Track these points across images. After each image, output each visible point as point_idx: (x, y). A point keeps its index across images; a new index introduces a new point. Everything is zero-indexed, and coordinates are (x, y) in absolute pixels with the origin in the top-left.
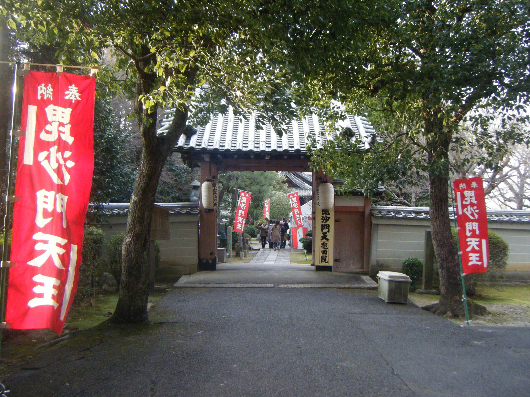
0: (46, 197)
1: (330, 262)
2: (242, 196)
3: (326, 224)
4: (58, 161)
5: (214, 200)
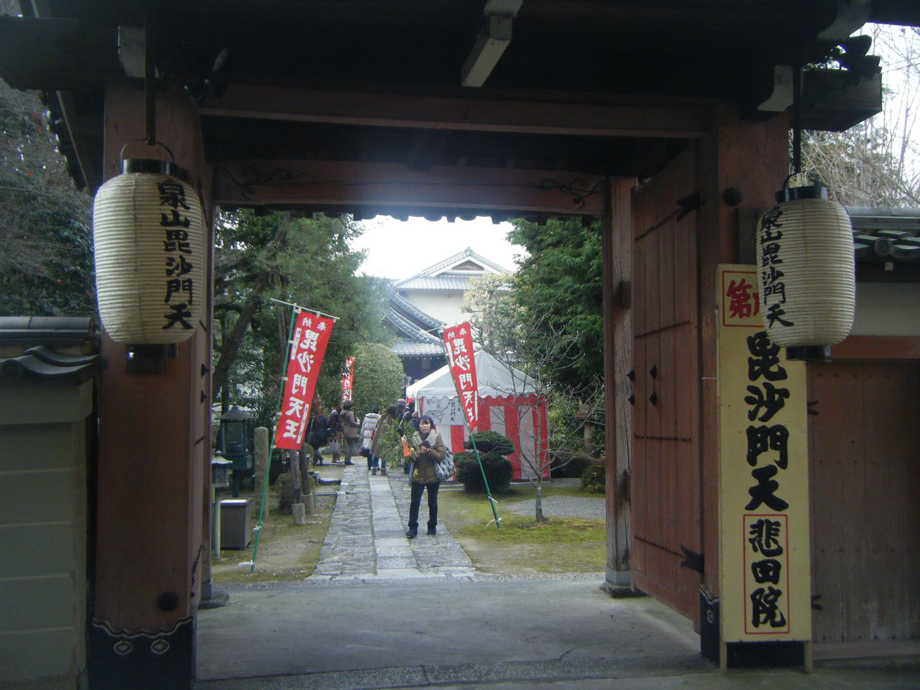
1: (798, 624)
2: (305, 328)
3: (769, 424)
5: (173, 287)
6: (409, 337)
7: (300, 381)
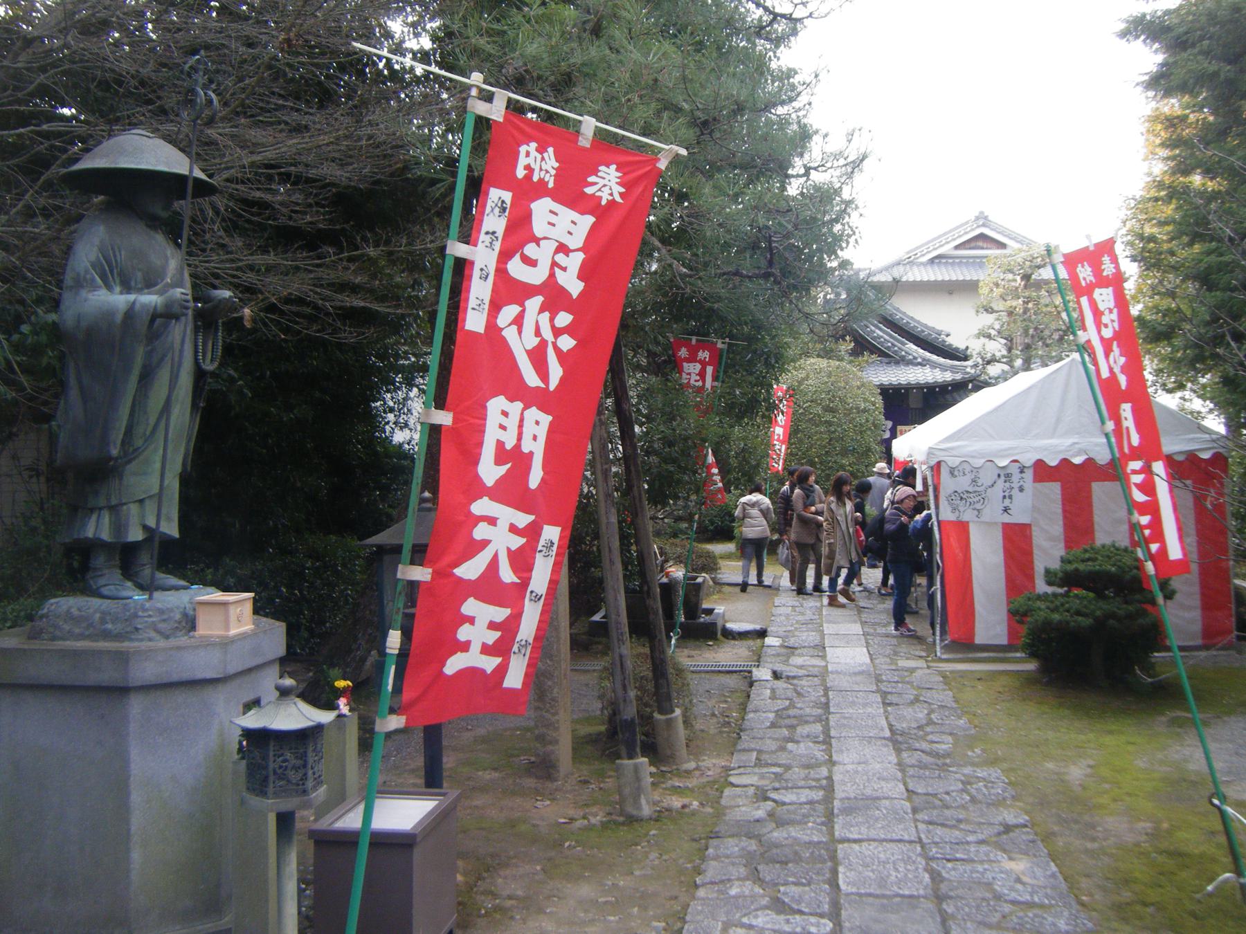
0: (505, 414)
2: (529, 190)
4: (538, 333)
6: (887, 356)
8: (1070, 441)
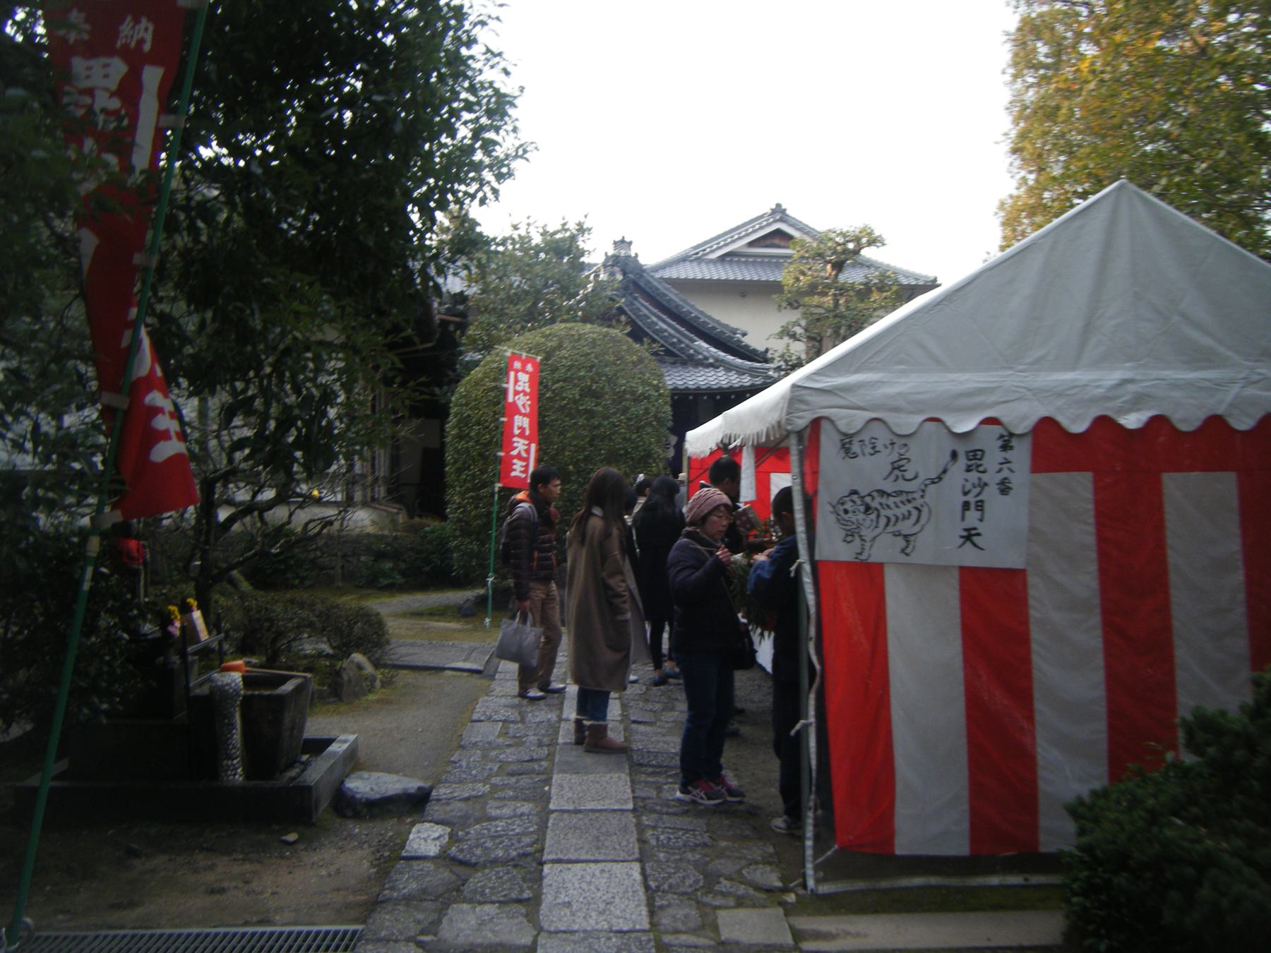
7: (521, 422)
8: (1117, 376)
